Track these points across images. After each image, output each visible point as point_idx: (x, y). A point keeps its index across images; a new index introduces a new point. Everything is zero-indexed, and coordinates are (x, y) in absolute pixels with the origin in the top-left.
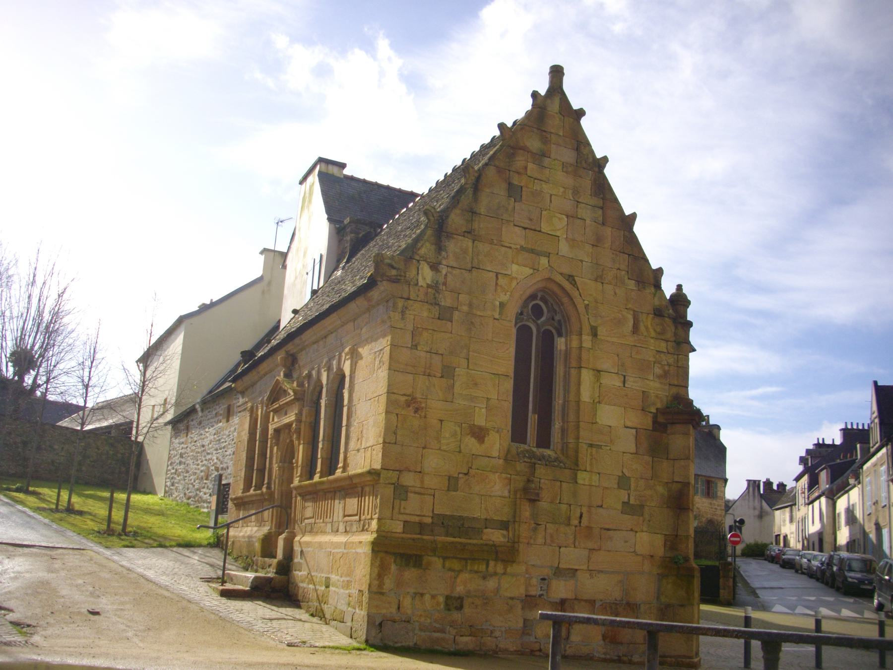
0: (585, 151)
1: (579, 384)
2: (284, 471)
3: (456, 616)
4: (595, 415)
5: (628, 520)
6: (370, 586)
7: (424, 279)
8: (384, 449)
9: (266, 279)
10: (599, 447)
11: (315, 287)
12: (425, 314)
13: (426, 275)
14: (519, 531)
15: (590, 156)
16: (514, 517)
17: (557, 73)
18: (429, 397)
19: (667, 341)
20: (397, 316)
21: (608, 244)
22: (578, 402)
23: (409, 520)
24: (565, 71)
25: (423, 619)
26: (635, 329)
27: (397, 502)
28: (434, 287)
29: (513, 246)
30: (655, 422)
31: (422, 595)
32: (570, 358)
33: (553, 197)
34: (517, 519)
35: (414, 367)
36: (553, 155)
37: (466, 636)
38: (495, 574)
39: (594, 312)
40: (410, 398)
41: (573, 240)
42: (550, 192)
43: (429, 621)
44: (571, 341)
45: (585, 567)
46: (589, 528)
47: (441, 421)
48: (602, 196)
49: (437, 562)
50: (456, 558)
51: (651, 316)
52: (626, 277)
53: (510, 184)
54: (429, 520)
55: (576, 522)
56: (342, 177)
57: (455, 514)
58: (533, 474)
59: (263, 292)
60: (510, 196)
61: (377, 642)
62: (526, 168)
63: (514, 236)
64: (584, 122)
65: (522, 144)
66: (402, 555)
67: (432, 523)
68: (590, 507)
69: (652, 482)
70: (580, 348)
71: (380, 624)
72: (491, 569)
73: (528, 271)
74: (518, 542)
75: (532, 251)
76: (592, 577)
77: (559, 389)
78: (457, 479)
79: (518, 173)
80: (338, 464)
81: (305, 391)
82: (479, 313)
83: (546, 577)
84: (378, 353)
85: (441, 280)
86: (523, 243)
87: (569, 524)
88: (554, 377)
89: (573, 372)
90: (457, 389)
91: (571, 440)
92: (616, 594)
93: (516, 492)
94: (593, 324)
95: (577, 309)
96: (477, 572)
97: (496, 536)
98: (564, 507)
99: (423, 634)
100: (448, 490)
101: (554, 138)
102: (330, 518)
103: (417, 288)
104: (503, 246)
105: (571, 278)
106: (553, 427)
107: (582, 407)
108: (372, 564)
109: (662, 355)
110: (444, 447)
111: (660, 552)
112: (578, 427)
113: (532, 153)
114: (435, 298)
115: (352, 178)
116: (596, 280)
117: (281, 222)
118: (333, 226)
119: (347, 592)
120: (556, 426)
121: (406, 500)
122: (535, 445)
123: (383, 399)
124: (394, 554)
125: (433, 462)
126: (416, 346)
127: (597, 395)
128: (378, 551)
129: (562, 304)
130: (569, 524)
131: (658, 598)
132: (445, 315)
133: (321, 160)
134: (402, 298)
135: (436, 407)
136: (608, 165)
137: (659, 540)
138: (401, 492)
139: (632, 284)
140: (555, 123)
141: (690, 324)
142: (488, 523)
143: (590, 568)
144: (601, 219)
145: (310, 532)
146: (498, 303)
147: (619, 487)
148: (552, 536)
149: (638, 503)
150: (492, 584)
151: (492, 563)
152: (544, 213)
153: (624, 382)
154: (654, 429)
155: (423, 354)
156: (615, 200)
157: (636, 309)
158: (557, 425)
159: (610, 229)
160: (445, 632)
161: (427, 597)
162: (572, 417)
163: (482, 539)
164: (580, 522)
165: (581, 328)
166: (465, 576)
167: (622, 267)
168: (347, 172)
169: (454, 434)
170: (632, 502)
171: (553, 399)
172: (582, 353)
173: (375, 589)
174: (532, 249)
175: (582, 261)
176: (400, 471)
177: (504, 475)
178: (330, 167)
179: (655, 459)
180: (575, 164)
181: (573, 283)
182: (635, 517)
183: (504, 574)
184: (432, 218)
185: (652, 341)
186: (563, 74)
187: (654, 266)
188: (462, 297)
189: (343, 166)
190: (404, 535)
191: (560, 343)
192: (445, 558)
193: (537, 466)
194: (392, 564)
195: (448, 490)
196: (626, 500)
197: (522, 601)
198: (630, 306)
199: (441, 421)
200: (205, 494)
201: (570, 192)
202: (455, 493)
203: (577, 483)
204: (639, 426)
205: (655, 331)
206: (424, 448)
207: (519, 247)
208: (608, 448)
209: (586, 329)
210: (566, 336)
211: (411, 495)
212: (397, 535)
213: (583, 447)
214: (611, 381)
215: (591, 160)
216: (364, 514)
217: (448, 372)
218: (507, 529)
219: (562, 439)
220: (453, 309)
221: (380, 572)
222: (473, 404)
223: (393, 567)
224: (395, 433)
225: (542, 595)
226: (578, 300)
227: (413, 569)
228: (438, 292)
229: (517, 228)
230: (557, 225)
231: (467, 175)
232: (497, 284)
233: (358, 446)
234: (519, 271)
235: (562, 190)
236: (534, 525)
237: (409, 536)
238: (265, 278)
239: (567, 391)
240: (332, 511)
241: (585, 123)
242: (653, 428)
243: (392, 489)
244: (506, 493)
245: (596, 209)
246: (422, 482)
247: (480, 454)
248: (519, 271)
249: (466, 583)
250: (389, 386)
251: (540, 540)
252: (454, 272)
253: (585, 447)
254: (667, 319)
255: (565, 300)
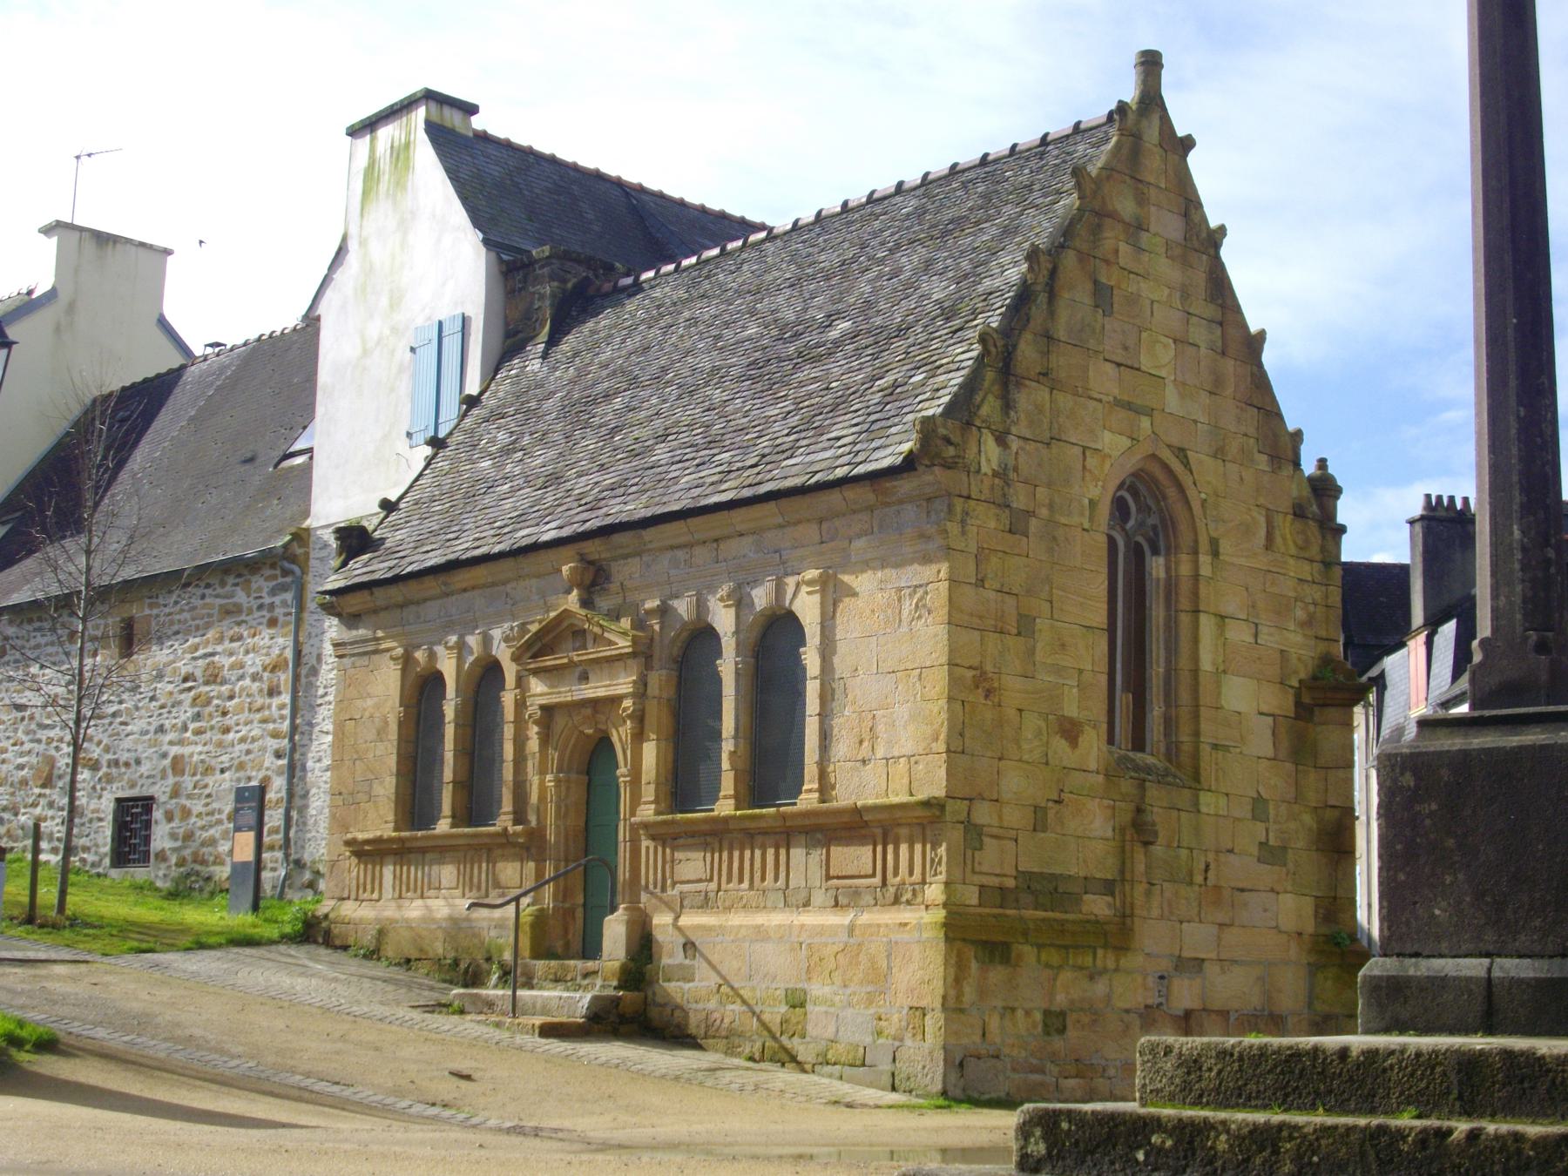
0: (1196, 218)
1: (1196, 640)
2: (568, 789)
3: (1058, 1043)
4: (1219, 694)
5: (1267, 874)
6: (944, 997)
7: (989, 461)
8: (949, 762)
9: (64, 297)
10: (1226, 748)
11: (473, 388)
12: (992, 524)
13: (990, 454)
14: (1132, 896)
15: (1203, 227)
16: (1122, 872)
17: (1150, 63)
18: (1003, 670)
19: (1312, 561)
20: (953, 528)
21: (1229, 391)
22: (1195, 672)
23: (986, 883)
24: (1164, 61)
25: (1015, 1052)
26: (1269, 543)
27: (969, 853)
28: (1001, 474)
29: (1104, 398)
30: (1298, 704)
31: (1013, 1010)
32: (1177, 594)
33: (1156, 306)
34: (1128, 876)
35: (981, 617)
36: (1152, 229)
37: (1072, 1077)
38: (1105, 970)
39: (1215, 513)
40: (978, 672)
41: (1184, 384)
42: (1151, 296)
43: (1023, 1054)
44: (1177, 563)
45: (1213, 955)
46: (1217, 888)
47: (1020, 710)
48: (1220, 301)
49: (1028, 952)
50: (1052, 945)
51: (1290, 517)
52: (1255, 450)
53: (1096, 282)
54: (1010, 883)
55: (1199, 879)
56: (471, 134)
57: (1045, 870)
58: (1143, 797)
59: (58, 329)
60: (1097, 306)
61: (958, 1093)
62: (1117, 251)
63: (1104, 380)
64: (1193, 159)
65: (1110, 208)
66: (984, 943)
67: (1017, 887)
68: (1218, 852)
69: (1296, 808)
70: (1196, 577)
71: (961, 1065)
72: (1099, 963)
73: (1125, 442)
74: (1132, 915)
75: (1129, 406)
76: (1223, 972)
77: (1158, 648)
78: (1045, 809)
79: (1107, 262)
80: (333, 745)
81: (652, 639)
82: (1063, 520)
83: (1166, 974)
84: (907, 591)
85: (1011, 462)
86: (1116, 391)
87: (1191, 883)
88: (1148, 625)
89: (1185, 619)
90: (1039, 656)
91: (1185, 738)
92: (1255, 1001)
93: (1123, 830)
94: (1213, 534)
95: (1190, 509)
96: (1081, 968)
97: (1098, 906)
98: (1184, 853)
99: (1016, 1076)
100: (1035, 830)
101: (1153, 192)
102: (776, 879)
103: (979, 477)
104: (1091, 398)
105: (1181, 453)
106: (1149, 716)
107: (1202, 679)
108: (946, 964)
109: (1306, 586)
110: (1026, 757)
111: (1309, 927)
112: (1196, 716)
113: (1124, 223)
114: (1004, 495)
115: (483, 137)
116: (1215, 456)
117: (89, 155)
118: (493, 255)
119: (872, 1011)
120: (1155, 713)
121: (981, 849)
122: (1130, 746)
123: (938, 682)
124: (974, 942)
125: (1014, 783)
126: (982, 581)
127: (1221, 660)
128: (954, 939)
129: (1165, 498)
130: (1191, 883)
131: (1310, 1004)
132: (1017, 525)
133: (430, 96)
134: (960, 496)
135: (1013, 687)
136: (1225, 241)
137: (1308, 905)
138: (974, 835)
139: (1262, 461)
140: (1154, 164)
141: (1342, 530)
142: (1088, 883)
143: (1223, 957)
144: (1219, 344)
145: (702, 907)
146: (1086, 501)
147: (1254, 818)
148: (1170, 905)
149: (1279, 844)
150: (1100, 988)
151: (1100, 952)
152: (1144, 335)
153: (1256, 636)
154: (1297, 717)
155: (992, 595)
156: (1237, 309)
157: (1271, 507)
158: (1156, 712)
159: (1232, 362)
160: (1044, 1073)
161: (1020, 1013)
162: (1185, 696)
163: (1081, 912)
164: (1206, 879)
165: (1196, 541)
166: (1066, 976)
167: (1252, 431)
168: (478, 123)
169: (1039, 733)
170: (1272, 842)
171: (1148, 665)
172: (1201, 586)
173: (951, 1003)
174: (1129, 403)
175: (1195, 422)
176: (971, 800)
177: (1106, 802)
178: (447, 111)
179: (1300, 767)
180: (1183, 242)
181: (1186, 464)
182: (1276, 868)
183: (1117, 970)
184: (993, 350)
185: (1292, 561)
186: (1162, 66)
187: (1291, 426)
188: (1041, 492)
189: (471, 109)
190: (980, 910)
191: (1157, 567)
192: (1040, 947)
193: (1147, 784)
194: (973, 961)
195: (1035, 830)
196: (1263, 840)
197: (1141, 1016)
198: (1261, 501)
199: (1020, 710)
200: (53, 818)
201: (1178, 294)
202: (1043, 835)
203: (1199, 811)
204: (1278, 712)
205: (1295, 542)
206: (1000, 759)
207: (1111, 399)
208: (1238, 750)
209: (1204, 545)
210: (1168, 554)
211: (986, 840)
212: (972, 910)
213: (1205, 750)
214: (1239, 634)
215: (1204, 235)
216: (896, 874)
217: (1026, 625)
218: (1112, 894)
219: (1167, 735)
220: (1029, 514)
221: (957, 975)
222: (1061, 681)
223: (974, 965)
224: (961, 735)
225: (1161, 1004)
226: (1191, 493)
227: (999, 968)
228: (1008, 485)
229: (1108, 364)
230: (1159, 357)
231: (1036, 267)
232: (1084, 467)
233: (865, 751)
234: (1112, 442)
235: (1167, 291)
236: (1147, 886)
237: (987, 910)
238: (59, 290)
239: (1172, 649)
240: (782, 868)
241: (1195, 161)
242: (1296, 712)
243: (962, 832)
244: (1110, 834)
245: (1214, 325)
246: (1000, 818)
247: (1073, 766)
248: (1112, 442)
249: (1068, 989)
250: (951, 651)
251: (1155, 912)
252: (1028, 447)
253: (1208, 748)
254: (1311, 522)
255: (1172, 492)
